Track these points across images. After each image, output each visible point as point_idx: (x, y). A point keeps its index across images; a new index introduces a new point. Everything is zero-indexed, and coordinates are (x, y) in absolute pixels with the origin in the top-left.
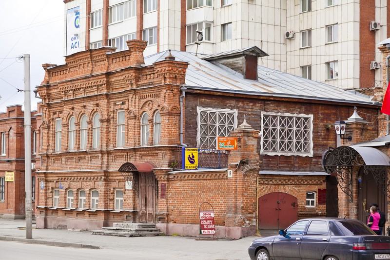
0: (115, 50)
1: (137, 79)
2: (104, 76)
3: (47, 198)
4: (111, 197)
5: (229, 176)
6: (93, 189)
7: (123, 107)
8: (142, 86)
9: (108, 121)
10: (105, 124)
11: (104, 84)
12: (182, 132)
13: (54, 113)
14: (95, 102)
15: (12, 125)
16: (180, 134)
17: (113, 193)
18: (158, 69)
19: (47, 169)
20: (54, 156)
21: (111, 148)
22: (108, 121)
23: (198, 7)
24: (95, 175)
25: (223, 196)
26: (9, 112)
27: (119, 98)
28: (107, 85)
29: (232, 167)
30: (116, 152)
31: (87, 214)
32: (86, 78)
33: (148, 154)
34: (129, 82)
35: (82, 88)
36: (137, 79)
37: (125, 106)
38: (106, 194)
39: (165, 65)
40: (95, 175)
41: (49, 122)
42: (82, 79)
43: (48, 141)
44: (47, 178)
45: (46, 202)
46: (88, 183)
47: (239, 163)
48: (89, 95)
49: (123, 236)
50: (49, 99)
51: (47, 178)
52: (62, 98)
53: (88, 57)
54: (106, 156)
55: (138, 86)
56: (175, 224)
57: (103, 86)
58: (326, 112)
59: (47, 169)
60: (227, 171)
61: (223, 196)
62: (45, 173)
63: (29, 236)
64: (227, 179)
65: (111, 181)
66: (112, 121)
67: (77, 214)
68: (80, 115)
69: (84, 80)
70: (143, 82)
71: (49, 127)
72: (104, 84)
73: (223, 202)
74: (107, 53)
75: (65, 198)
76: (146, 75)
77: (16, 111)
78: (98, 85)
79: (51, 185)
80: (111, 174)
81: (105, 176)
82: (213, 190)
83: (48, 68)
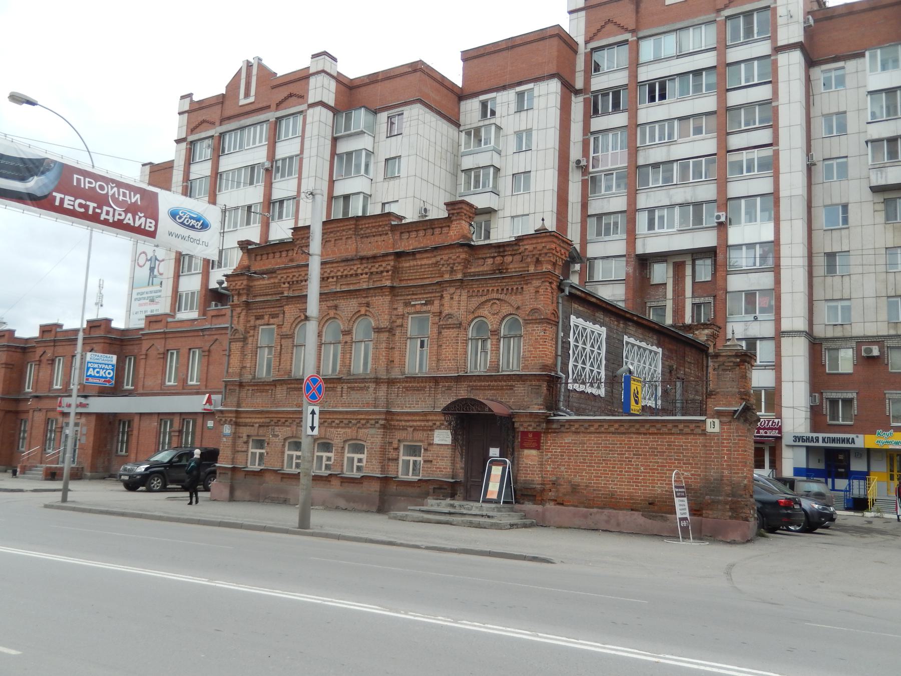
0: (401, 220)
1: (467, 263)
2: (393, 257)
3: (235, 452)
4: (393, 454)
5: (709, 429)
6: (289, 437)
7: (428, 308)
8: (471, 276)
9: (391, 331)
10: (384, 336)
11: (387, 271)
12: (559, 353)
13: (258, 318)
14: (364, 301)
15: (94, 345)
16: (557, 355)
17: (397, 449)
18: (527, 247)
19: (239, 405)
20: (254, 385)
21: (396, 374)
22: (391, 331)
23: (834, 89)
24: (363, 417)
25: (691, 464)
26: (91, 327)
27: (416, 294)
28: (394, 272)
29: (719, 414)
30: (407, 382)
31: (335, 482)
32: (347, 260)
33: (489, 386)
34: (449, 269)
35: (333, 278)
36: (467, 263)
37: (435, 307)
38: (383, 450)
39: (545, 240)
40: (363, 417)
41: (247, 332)
42: (337, 262)
43: (242, 361)
44: (239, 420)
45: (233, 458)
46: (285, 429)
47: (740, 408)
48: (352, 288)
49: (451, 524)
50: (248, 295)
51: (239, 420)
52: (283, 293)
53: (350, 229)
54: (384, 388)
55: (465, 275)
56: (558, 507)
57: (385, 274)
58: (670, 346)
59: (239, 405)
60: (704, 421)
61: (691, 464)
62: (237, 412)
63: (304, 523)
64: (705, 434)
65: (395, 428)
66: (398, 332)
67: (282, 478)
68: (297, 322)
69: (343, 264)
70: (473, 270)
71: (244, 340)
72: (387, 271)
73: (692, 475)
74: (393, 223)
75: (283, 453)
76: (484, 259)
77: (102, 327)
78: (372, 273)
79: (244, 431)
80: (395, 417)
81: (385, 419)
82: (664, 452)
83: (250, 247)
